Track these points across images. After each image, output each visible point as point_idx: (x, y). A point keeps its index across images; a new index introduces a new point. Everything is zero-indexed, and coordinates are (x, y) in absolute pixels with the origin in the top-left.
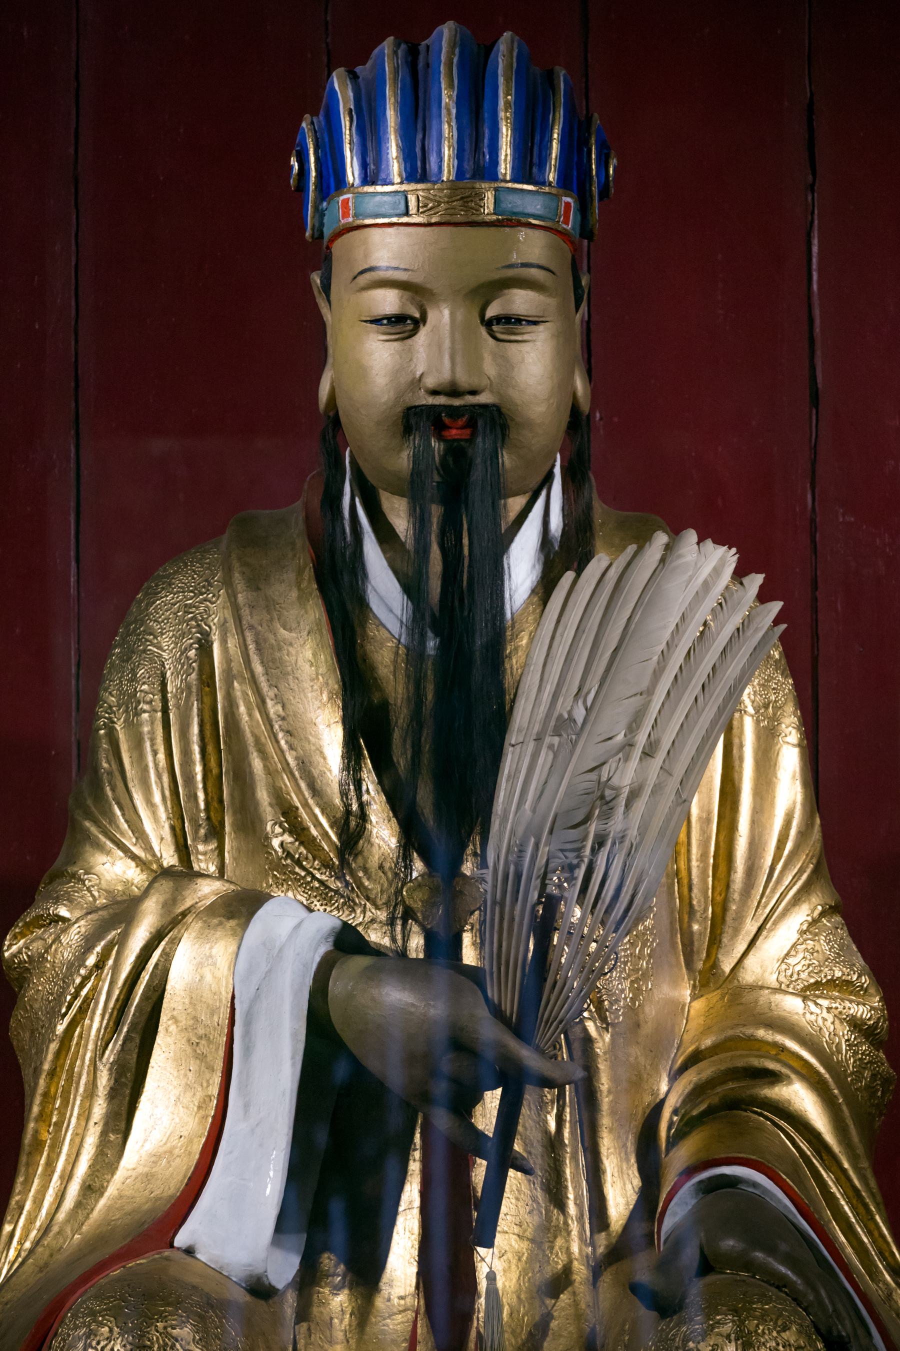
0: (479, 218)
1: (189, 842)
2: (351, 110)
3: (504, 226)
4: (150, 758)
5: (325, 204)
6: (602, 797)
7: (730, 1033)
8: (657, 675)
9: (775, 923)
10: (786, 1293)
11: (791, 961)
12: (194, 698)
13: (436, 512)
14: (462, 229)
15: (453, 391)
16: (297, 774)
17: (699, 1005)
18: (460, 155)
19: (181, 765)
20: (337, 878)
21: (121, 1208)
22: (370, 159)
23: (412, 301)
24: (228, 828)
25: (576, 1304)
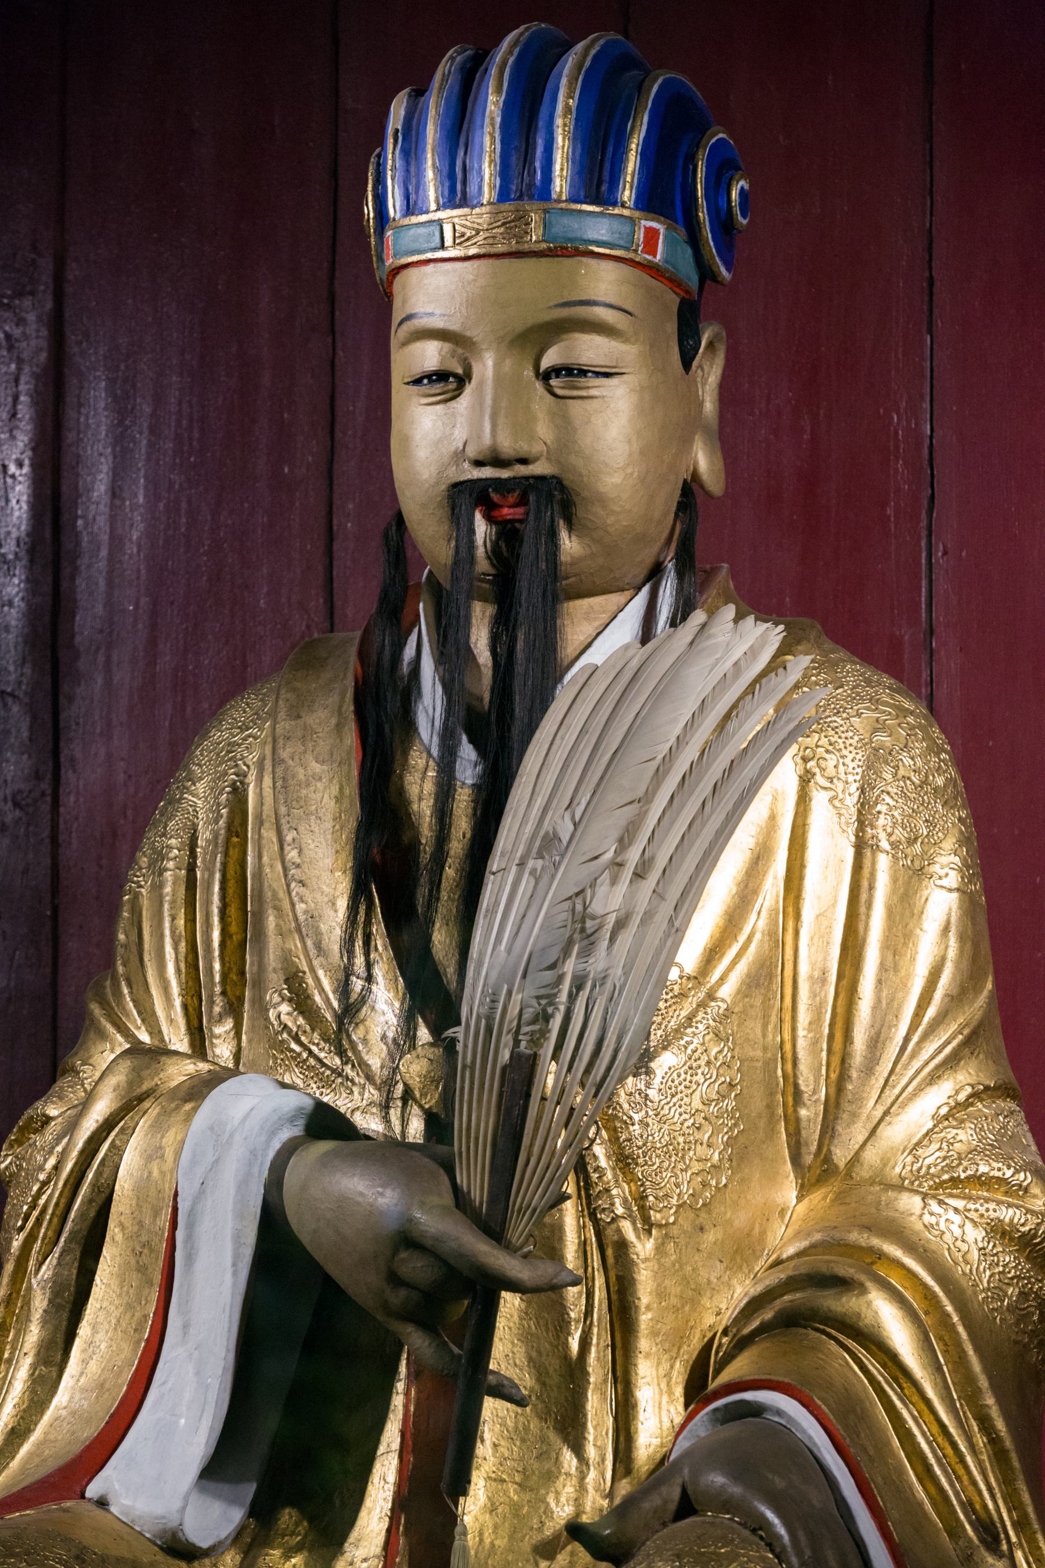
2: (397, 131)
3: (558, 256)
6: (583, 930)
8: (659, 776)
9: (904, 1106)
10: (761, 1538)
14: (506, 261)
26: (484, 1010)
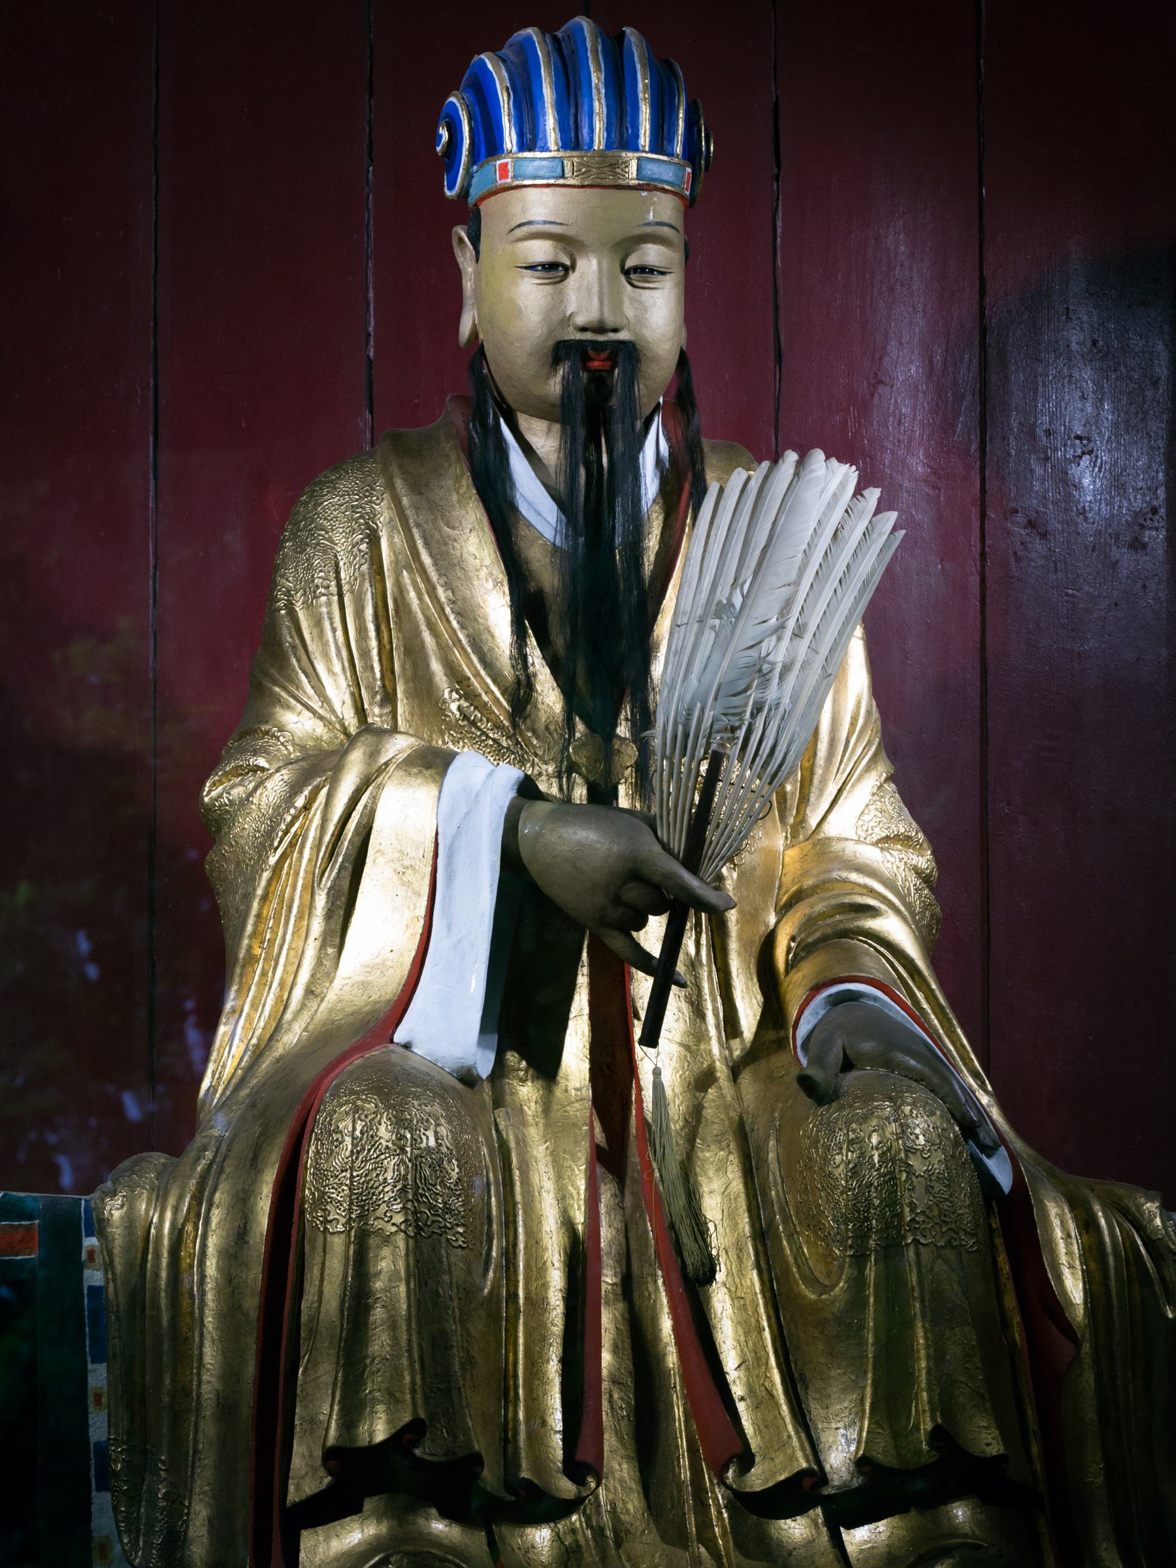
0: (621, 182)
1: (366, 706)
4: (329, 634)
5: (475, 167)
6: (760, 670)
7: (822, 877)
11: (866, 818)
12: (367, 584)
13: (581, 432)
15: (600, 328)
16: (469, 650)
17: (792, 854)
18: (608, 129)
19: (357, 641)
20: (508, 737)
21: (343, 1010)
22: (526, 129)
23: (564, 250)
24: (400, 695)
25: (722, 1096)
26: (681, 720)
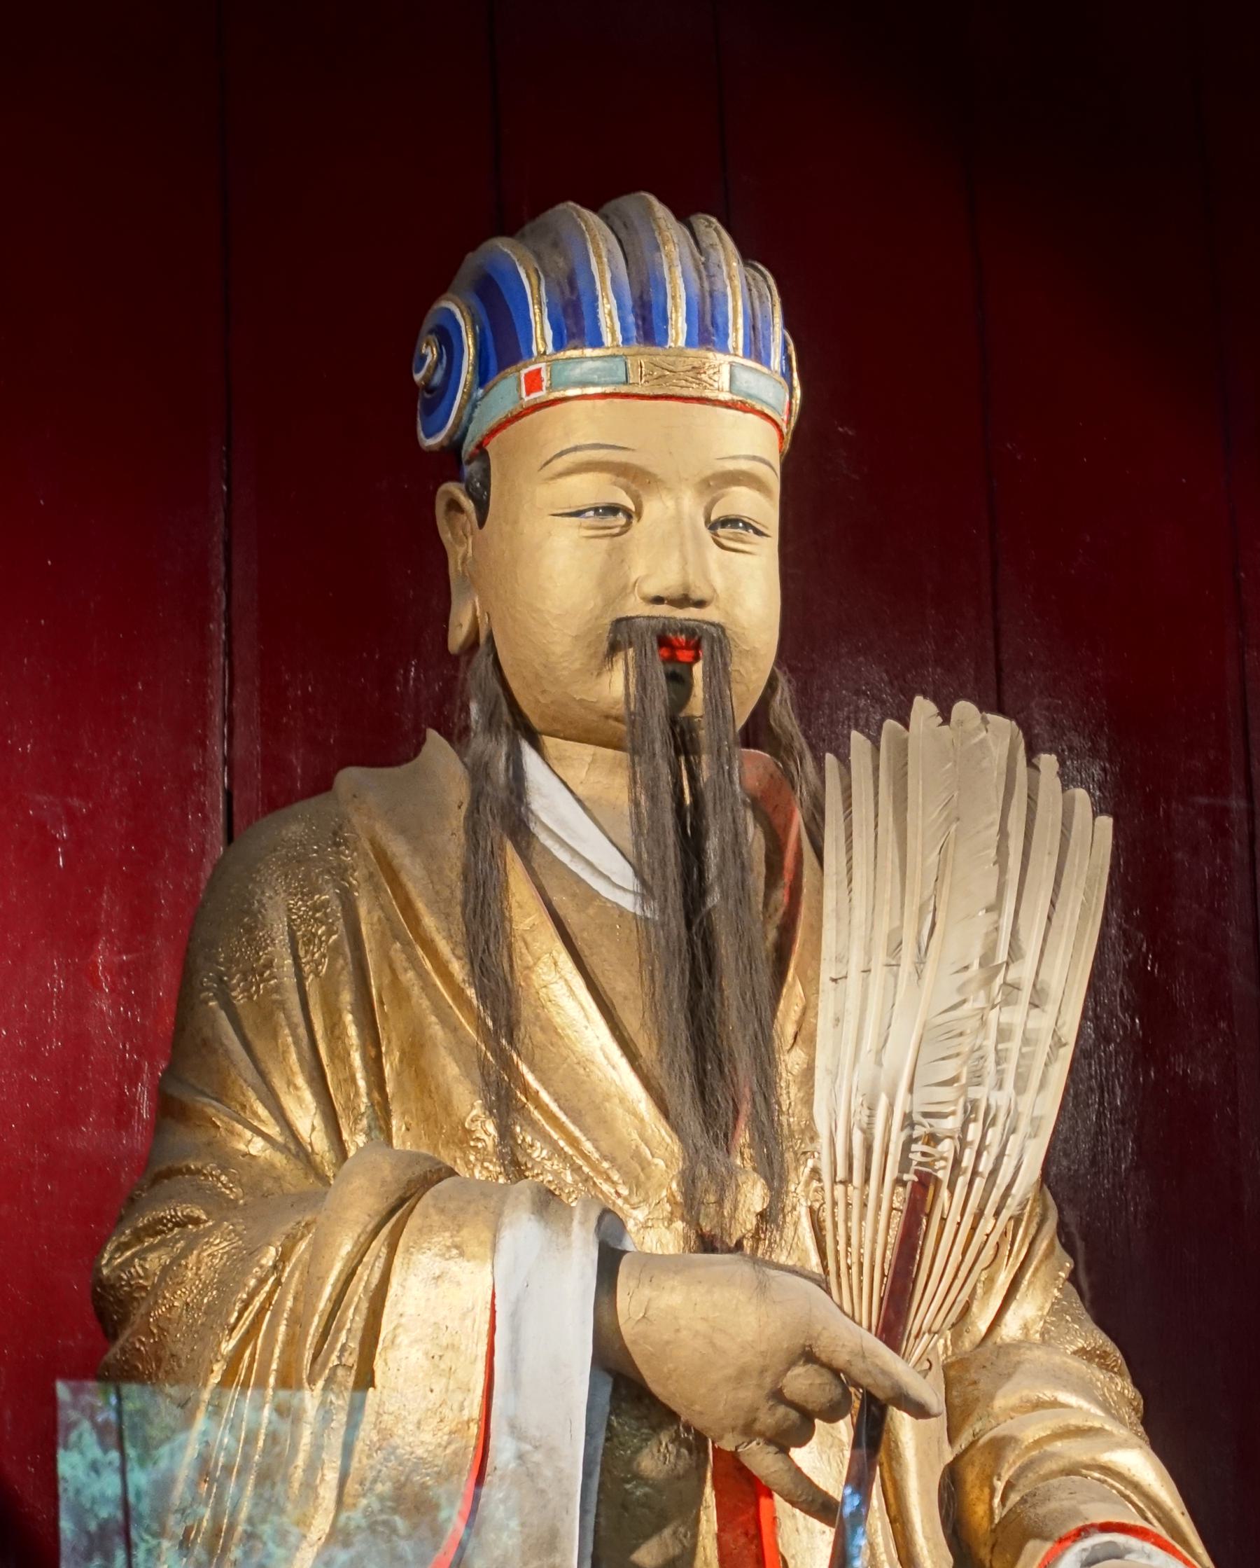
15: (684, 601)
